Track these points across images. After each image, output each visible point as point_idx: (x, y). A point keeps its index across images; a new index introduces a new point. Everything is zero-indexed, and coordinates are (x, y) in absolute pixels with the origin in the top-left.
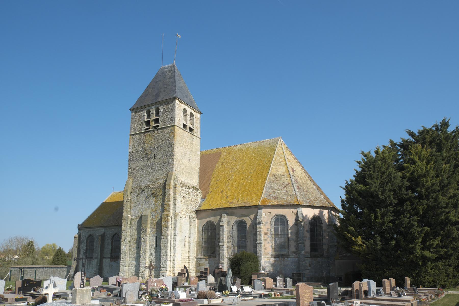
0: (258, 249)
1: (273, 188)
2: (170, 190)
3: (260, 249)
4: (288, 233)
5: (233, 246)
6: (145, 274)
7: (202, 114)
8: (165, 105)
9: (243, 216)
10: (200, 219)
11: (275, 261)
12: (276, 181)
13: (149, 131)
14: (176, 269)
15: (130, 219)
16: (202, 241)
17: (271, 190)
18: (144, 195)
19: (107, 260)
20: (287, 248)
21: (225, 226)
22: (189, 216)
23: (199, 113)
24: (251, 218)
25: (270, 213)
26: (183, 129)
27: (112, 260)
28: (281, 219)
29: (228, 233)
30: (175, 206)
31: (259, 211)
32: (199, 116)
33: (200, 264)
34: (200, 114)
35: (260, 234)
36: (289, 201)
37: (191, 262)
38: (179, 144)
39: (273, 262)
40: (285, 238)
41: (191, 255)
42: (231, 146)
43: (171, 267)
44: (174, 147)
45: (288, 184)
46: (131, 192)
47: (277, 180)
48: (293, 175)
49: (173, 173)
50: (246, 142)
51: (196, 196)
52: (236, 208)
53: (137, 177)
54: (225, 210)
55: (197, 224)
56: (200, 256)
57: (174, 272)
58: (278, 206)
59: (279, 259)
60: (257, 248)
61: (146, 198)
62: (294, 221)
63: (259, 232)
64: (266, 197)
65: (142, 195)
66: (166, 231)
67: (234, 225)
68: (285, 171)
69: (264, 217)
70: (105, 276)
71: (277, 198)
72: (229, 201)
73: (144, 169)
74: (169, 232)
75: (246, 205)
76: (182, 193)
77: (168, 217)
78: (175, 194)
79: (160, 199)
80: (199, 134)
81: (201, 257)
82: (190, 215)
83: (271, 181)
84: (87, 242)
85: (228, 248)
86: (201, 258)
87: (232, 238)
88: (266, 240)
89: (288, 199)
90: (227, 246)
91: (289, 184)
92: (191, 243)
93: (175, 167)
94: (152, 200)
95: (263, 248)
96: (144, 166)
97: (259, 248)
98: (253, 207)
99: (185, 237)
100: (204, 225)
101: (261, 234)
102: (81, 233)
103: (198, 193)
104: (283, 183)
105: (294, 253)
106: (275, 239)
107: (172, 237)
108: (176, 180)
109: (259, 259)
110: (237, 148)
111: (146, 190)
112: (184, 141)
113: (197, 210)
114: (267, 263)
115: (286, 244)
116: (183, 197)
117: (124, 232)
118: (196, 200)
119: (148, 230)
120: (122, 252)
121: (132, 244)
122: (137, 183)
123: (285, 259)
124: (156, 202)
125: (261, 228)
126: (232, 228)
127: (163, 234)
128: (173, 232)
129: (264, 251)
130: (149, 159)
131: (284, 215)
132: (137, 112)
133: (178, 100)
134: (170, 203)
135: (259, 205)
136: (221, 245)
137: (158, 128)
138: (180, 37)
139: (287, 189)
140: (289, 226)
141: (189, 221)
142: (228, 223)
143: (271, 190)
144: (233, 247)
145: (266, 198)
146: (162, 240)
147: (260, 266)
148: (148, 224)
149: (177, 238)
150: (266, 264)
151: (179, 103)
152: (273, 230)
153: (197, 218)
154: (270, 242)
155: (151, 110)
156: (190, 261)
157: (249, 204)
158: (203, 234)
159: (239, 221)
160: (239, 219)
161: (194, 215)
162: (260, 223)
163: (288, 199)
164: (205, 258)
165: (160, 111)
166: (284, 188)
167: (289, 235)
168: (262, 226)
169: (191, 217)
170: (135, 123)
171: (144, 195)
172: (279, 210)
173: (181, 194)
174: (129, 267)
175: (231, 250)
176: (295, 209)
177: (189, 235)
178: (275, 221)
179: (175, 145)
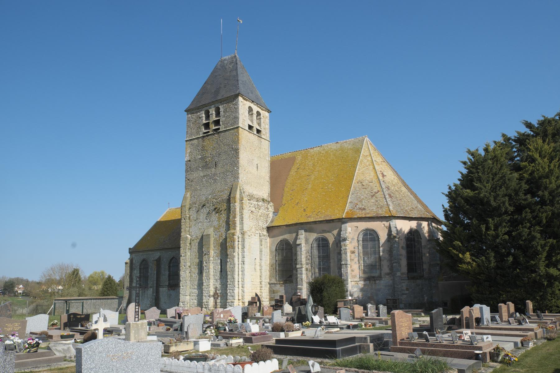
0: (343, 271)
1: (360, 197)
2: (236, 204)
5: (313, 268)
7: (271, 112)
8: (226, 103)
9: (324, 231)
10: (272, 237)
11: (364, 285)
13: (209, 135)
14: (245, 297)
15: (189, 239)
18: (205, 211)
19: (165, 289)
21: (303, 245)
24: (333, 235)
25: (357, 227)
26: (249, 130)
27: (170, 288)
28: (370, 234)
31: (343, 226)
32: (267, 114)
34: (269, 112)
35: (346, 253)
37: (263, 288)
38: (245, 149)
39: (363, 286)
40: (376, 257)
41: (263, 280)
43: (240, 295)
45: (377, 193)
46: (190, 208)
47: (363, 187)
48: (383, 181)
51: (266, 210)
52: (315, 222)
53: (196, 190)
54: (302, 226)
55: (269, 243)
56: (274, 281)
57: (243, 302)
58: (366, 218)
59: (370, 283)
60: (342, 269)
61: (207, 215)
63: (343, 251)
64: (351, 209)
66: (233, 253)
68: (374, 176)
69: (350, 233)
70: (163, 308)
71: (364, 209)
74: (236, 254)
77: (235, 236)
78: (242, 208)
79: (224, 215)
81: (275, 282)
82: (261, 232)
84: (140, 269)
86: (275, 284)
87: (312, 258)
88: (353, 260)
89: (378, 210)
91: (378, 191)
93: (241, 176)
94: (215, 217)
96: (204, 176)
97: (345, 270)
98: (336, 221)
99: (255, 259)
101: (347, 253)
103: (269, 206)
104: (372, 190)
105: (388, 274)
106: (364, 258)
107: (240, 260)
108: (242, 191)
109: (345, 283)
111: (207, 205)
113: (269, 226)
114: (355, 288)
115: (377, 264)
116: (252, 211)
117: (183, 255)
120: (181, 279)
121: (192, 270)
122: (196, 197)
124: (219, 219)
125: (346, 246)
126: (312, 247)
128: (240, 254)
132: (193, 113)
133: (242, 97)
135: (343, 218)
137: (219, 131)
138: (241, 22)
139: (376, 197)
141: (259, 241)
142: (307, 240)
146: (228, 263)
148: (211, 245)
150: (353, 289)
153: (269, 236)
154: (358, 262)
155: (210, 110)
158: (277, 254)
159: (320, 237)
160: (319, 235)
161: (265, 233)
162: (345, 240)
163: (378, 210)
164: (280, 284)
165: (220, 111)
167: (381, 254)
170: (192, 126)
171: (205, 210)
174: (190, 296)
175: (311, 273)
176: (387, 221)
179: (239, 150)
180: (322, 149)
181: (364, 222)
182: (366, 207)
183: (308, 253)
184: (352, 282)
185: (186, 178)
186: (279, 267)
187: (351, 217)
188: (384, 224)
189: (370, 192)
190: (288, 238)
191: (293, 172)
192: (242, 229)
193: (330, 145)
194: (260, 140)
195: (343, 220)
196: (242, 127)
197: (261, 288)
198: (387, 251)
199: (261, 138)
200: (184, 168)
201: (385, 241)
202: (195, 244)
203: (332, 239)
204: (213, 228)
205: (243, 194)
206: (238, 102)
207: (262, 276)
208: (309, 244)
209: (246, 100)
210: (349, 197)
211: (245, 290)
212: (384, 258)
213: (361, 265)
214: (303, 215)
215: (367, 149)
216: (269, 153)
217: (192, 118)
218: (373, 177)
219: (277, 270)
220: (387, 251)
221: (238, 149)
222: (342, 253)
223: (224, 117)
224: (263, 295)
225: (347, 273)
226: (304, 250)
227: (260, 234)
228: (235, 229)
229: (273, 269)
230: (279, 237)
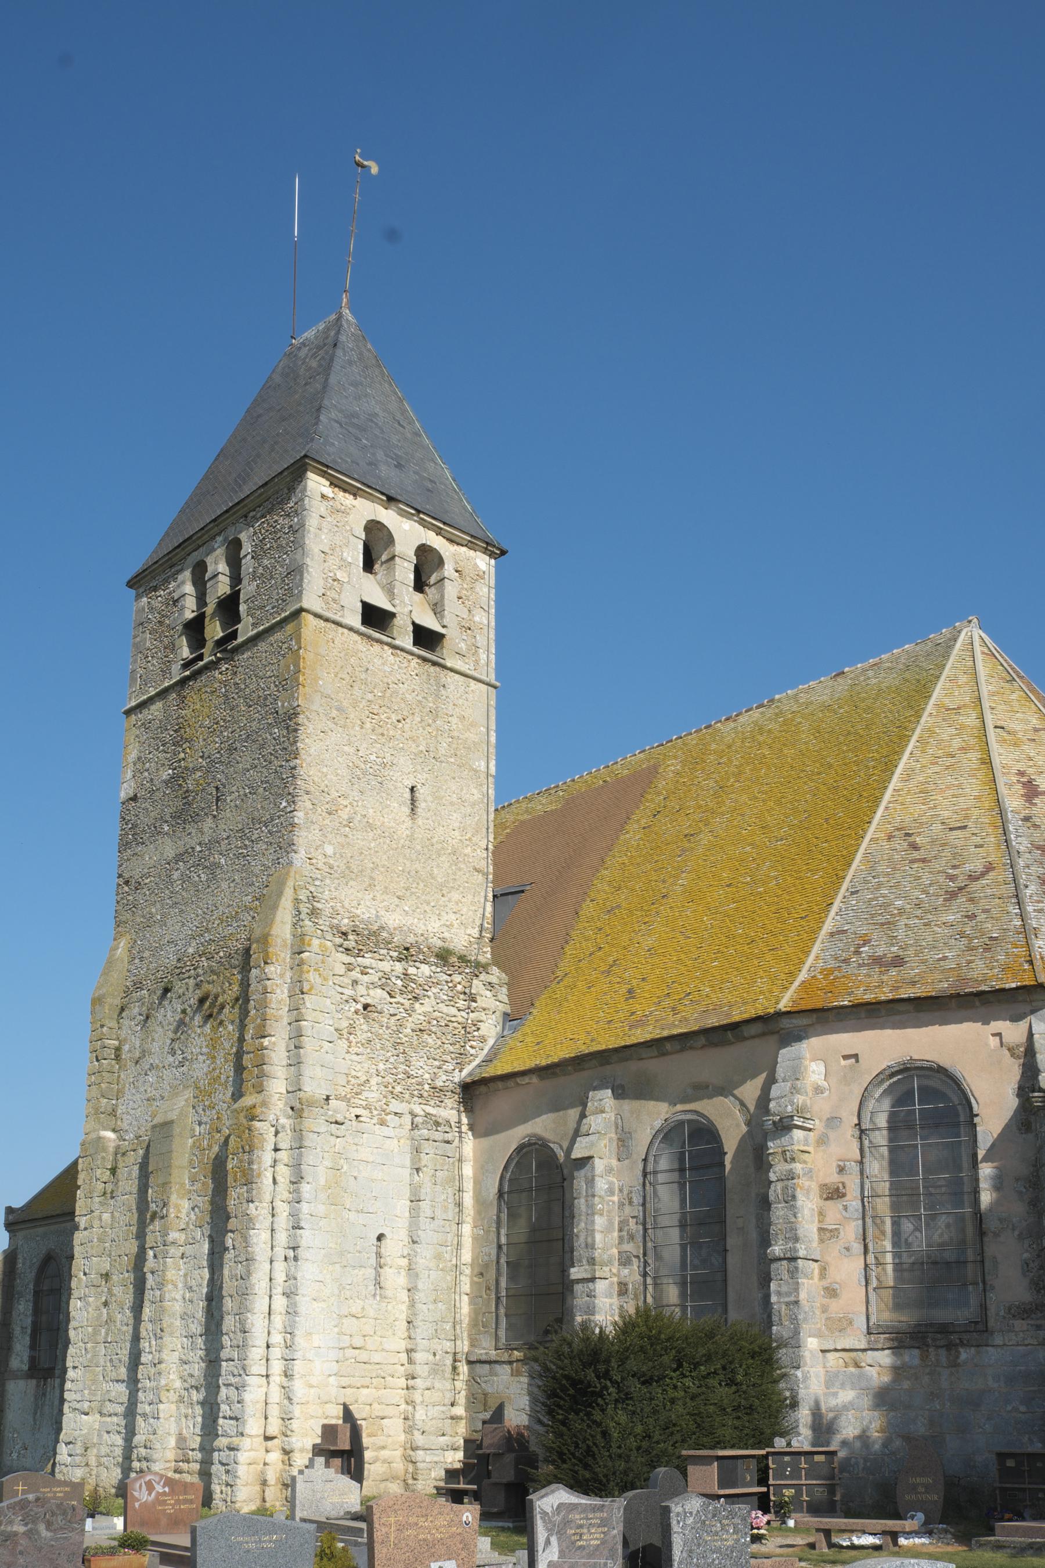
0: (779, 1293)
1: (886, 906)
2: (270, 969)
3: (789, 1294)
4: (977, 1180)
5: (649, 1280)
6: (156, 1456)
7: (503, 553)
9: (702, 1090)
10: (487, 1134)
11: (897, 1371)
12: (913, 861)
14: (295, 1425)
15: (111, 1150)
16: (498, 1262)
17: (873, 916)
18: (169, 1014)
20: (975, 1284)
21: (599, 1165)
22: (407, 1119)
23: (485, 551)
24: (742, 1104)
25: (856, 1056)
26: (363, 629)
28: (927, 1093)
29: (621, 1205)
30: (298, 1056)
31: (785, 1053)
32: (483, 562)
33: (485, 1395)
34: (492, 555)
35: (790, 1199)
36: (974, 974)
37: (418, 1382)
38: (334, 713)
39: (886, 1379)
40: (961, 1219)
41: (422, 1344)
42: (708, 727)
43: (274, 1412)
44: (296, 730)
45: (983, 874)
46: (122, 1009)
47: (916, 855)
48: (1027, 819)
49: (288, 873)
50: (785, 691)
51: (461, 1004)
52: (657, 1046)
53: (149, 923)
54: (608, 1070)
55: (476, 1160)
56: (487, 1349)
57: (287, 1447)
58: (901, 1007)
59: (924, 1358)
61: (176, 1032)
62: (1011, 1102)
63: (779, 1186)
64: (833, 964)
65: (160, 1018)
66: (245, 1205)
67: (653, 1152)
68: (978, 798)
69: (818, 1090)
71: (898, 962)
72: (633, 1013)
73: (176, 875)
74: (259, 1211)
75: (713, 1021)
76: (355, 982)
77: (257, 1124)
78: (299, 990)
80: (483, 662)
81: (493, 1354)
82: (418, 1110)
83: (880, 869)
85: (624, 1298)
86: (489, 1362)
87: (645, 1230)
88: (834, 1233)
89: (969, 962)
90: (620, 1283)
91: (989, 868)
92: (417, 1275)
93: (305, 839)
94: (199, 1035)
95: (809, 1287)
96: (179, 858)
97: (784, 1289)
99: (380, 1238)
100: (506, 1168)
101: (794, 1197)
102: (16, 1248)
103: (477, 986)
104: (954, 867)
105: (1024, 1312)
106: (896, 1224)
107: (282, 1238)
108: (304, 909)
109: (783, 1355)
110: (735, 728)
111: (179, 987)
112: (370, 696)
113: (468, 1080)
114: (843, 1386)
115: (970, 1255)
116: (366, 1007)
117: (82, 1226)
118: (469, 1030)
119: (178, 1207)
120: (72, 1334)
121: (115, 1290)
122: (146, 954)
123: (964, 1354)
124: (214, 1044)
125: (793, 1159)
126: (645, 1174)
127: (232, 1224)
128: (283, 1210)
129: (825, 1309)
130: (196, 818)
131: (945, 1062)
132: (155, 589)
133: (324, 474)
134: (266, 1042)
135: (779, 1014)
136: (579, 1276)
137: (235, 643)
138: (374, 169)
139: (972, 900)
140: (980, 1137)
141: (408, 1149)
142: (624, 1140)
143: (873, 916)
144: (650, 1288)
145: (831, 971)
147: (794, 1405)
148: (175, 1172)
149: (303, 1243)
150: (835, 1394)
151: (328, 491)
152: (878, 1168)
153: (471, 1127)
154: (857, 1248)
155: (209, 560)
156: (413, 1378)
157: (728, 1015)
158: (504, 1216)
159: (681, 1123)
160: (680, 1111)
161: (449, 1111)
162: (784, 1126)
163: (969, 962)
164: (510, 1363)
165: (243, 553)
166: (952, 895)
167: (986, 1198)
168: (796, 1148)
169: (417, 1120)
170: (148, 644)
171: (169, 1013)
172: (910, 1032)
173: (349, 992)
174: (101, 1414)
176: (1016, 1018)
177: (410, 1225)
178: (893, 1106)
179: (301, 719)
180: (770, 712)
181: (894, 1027)
182: (911, 952)
183: (631, 1203)
184: (831, 1356)
185: (120, 876)
186: (511, 1278)
187: (819, 1005)
188: (999, 1035)
189: (941, 879)
190: (548, 1135)
191: (632, 835)
192: (295, 1089)
193: (806, 691)
194: (437, 678)
195: (786, 1023)
196: (319, 611)
197: (411, 1382)
198: (1017, 1180)
199: (444, 667)
200: (114, 830)
201: (1007, 1126)
202: (130, 1173)
203: (738, 1125)
204: (189, 1094)
205: (307, 922)
206: (302, 500)
207: (418, 1322)
208: (634, 1156)
209: (355, 493)
210: (834, 909)
211: (298, 1387)
212: (1000, 1220)
213: (878, 1263)
214: (621, 1015)
215: (963, 679)
216: (493, 739)
217: (152, 609)
218: (971, 802)
219: (504, 1293)
220: (1017, 1180)
221: (296, 714)
222: (772, 1198)
223: (254, 579)
224: (418, 1416)
225: (797, 1302)
226: (610, 1191)
227: (414, 1115)
228: (260, 1090)
229: (488, 1288)
230: (510, 1132)
